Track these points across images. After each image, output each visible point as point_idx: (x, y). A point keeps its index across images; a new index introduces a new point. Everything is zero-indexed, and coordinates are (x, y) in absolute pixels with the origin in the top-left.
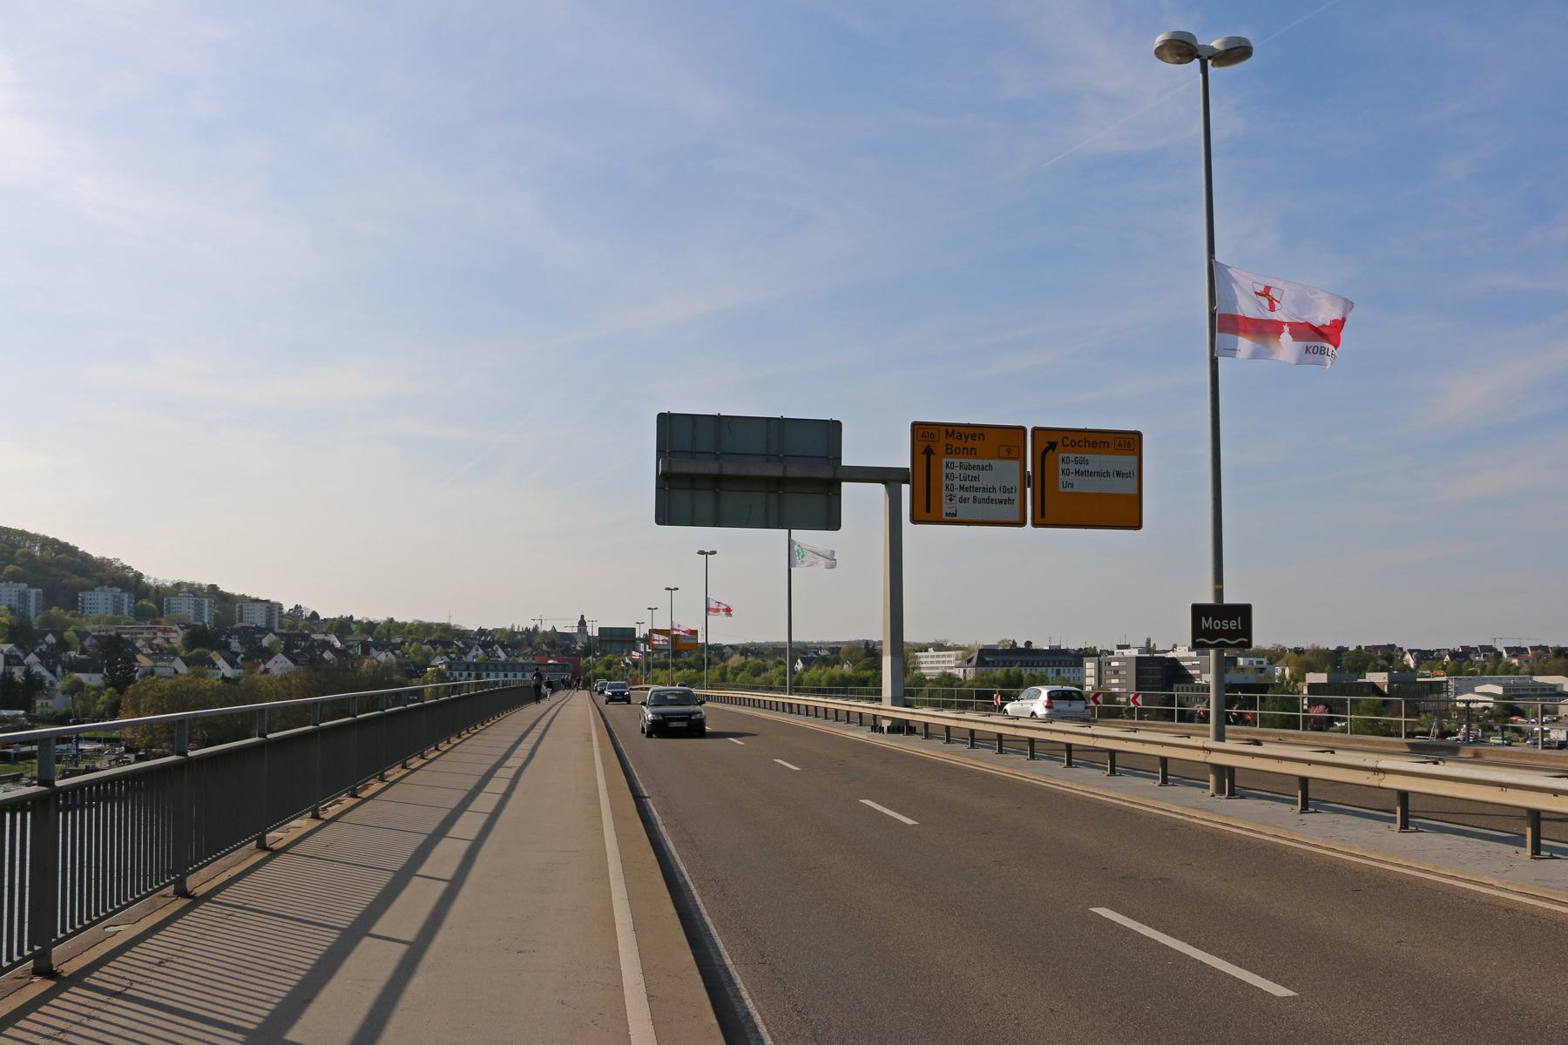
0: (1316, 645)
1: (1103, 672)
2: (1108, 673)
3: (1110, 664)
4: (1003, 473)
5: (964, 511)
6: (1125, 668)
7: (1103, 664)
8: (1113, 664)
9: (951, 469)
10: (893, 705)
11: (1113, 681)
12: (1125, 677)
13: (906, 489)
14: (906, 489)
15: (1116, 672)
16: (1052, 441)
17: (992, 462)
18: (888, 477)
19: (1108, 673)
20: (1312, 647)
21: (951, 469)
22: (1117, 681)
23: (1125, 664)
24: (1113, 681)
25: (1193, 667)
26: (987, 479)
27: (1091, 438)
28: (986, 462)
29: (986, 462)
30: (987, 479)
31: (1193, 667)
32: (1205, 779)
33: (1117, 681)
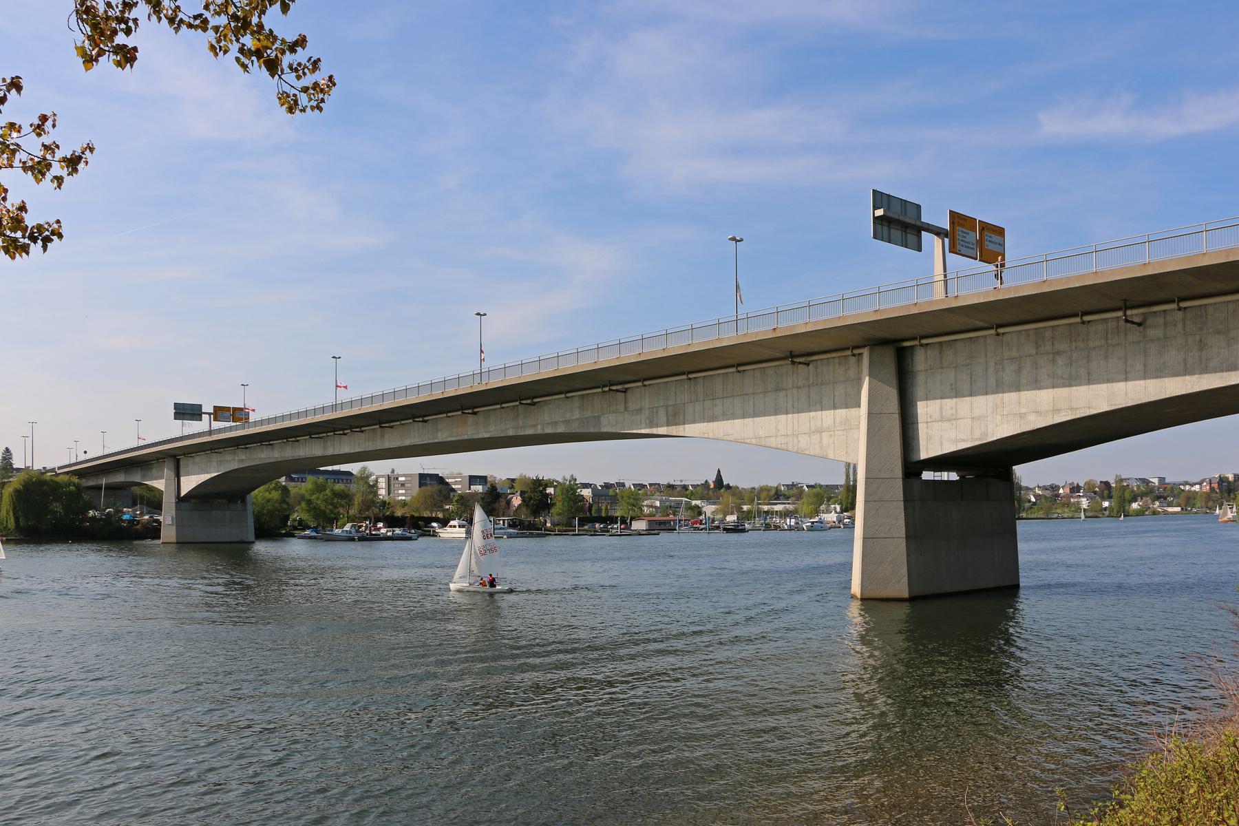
0: (524, 474)
1: (392, 485)
2: (397, 486)
3: (397, 479)
4: (227, 414)
5: (964, 251)
6: (410, 482)
7: (392, 479)
8: (400, 479)
9: (219, 413)
10: (859, 406)
11: (400, 492)
12: (410, 489)
13: (212, 416)
14: (212, 416)
15: (403, 485)
16: (235, 409)
17: (969, 231)
18: (210, 414)
19: (397, 486)
20: (521, 476)
21: (219, 413)
22: (404, 491)
23: (410, 478)
24: (400, 492)
25: (456, 483)
26: (225, 415)
27: (993, 228)
28: (967, 231)
29: (967, 231)
30: (225, 415)
31: (456, 483)
32: (870, 603)
33: (404, 491)
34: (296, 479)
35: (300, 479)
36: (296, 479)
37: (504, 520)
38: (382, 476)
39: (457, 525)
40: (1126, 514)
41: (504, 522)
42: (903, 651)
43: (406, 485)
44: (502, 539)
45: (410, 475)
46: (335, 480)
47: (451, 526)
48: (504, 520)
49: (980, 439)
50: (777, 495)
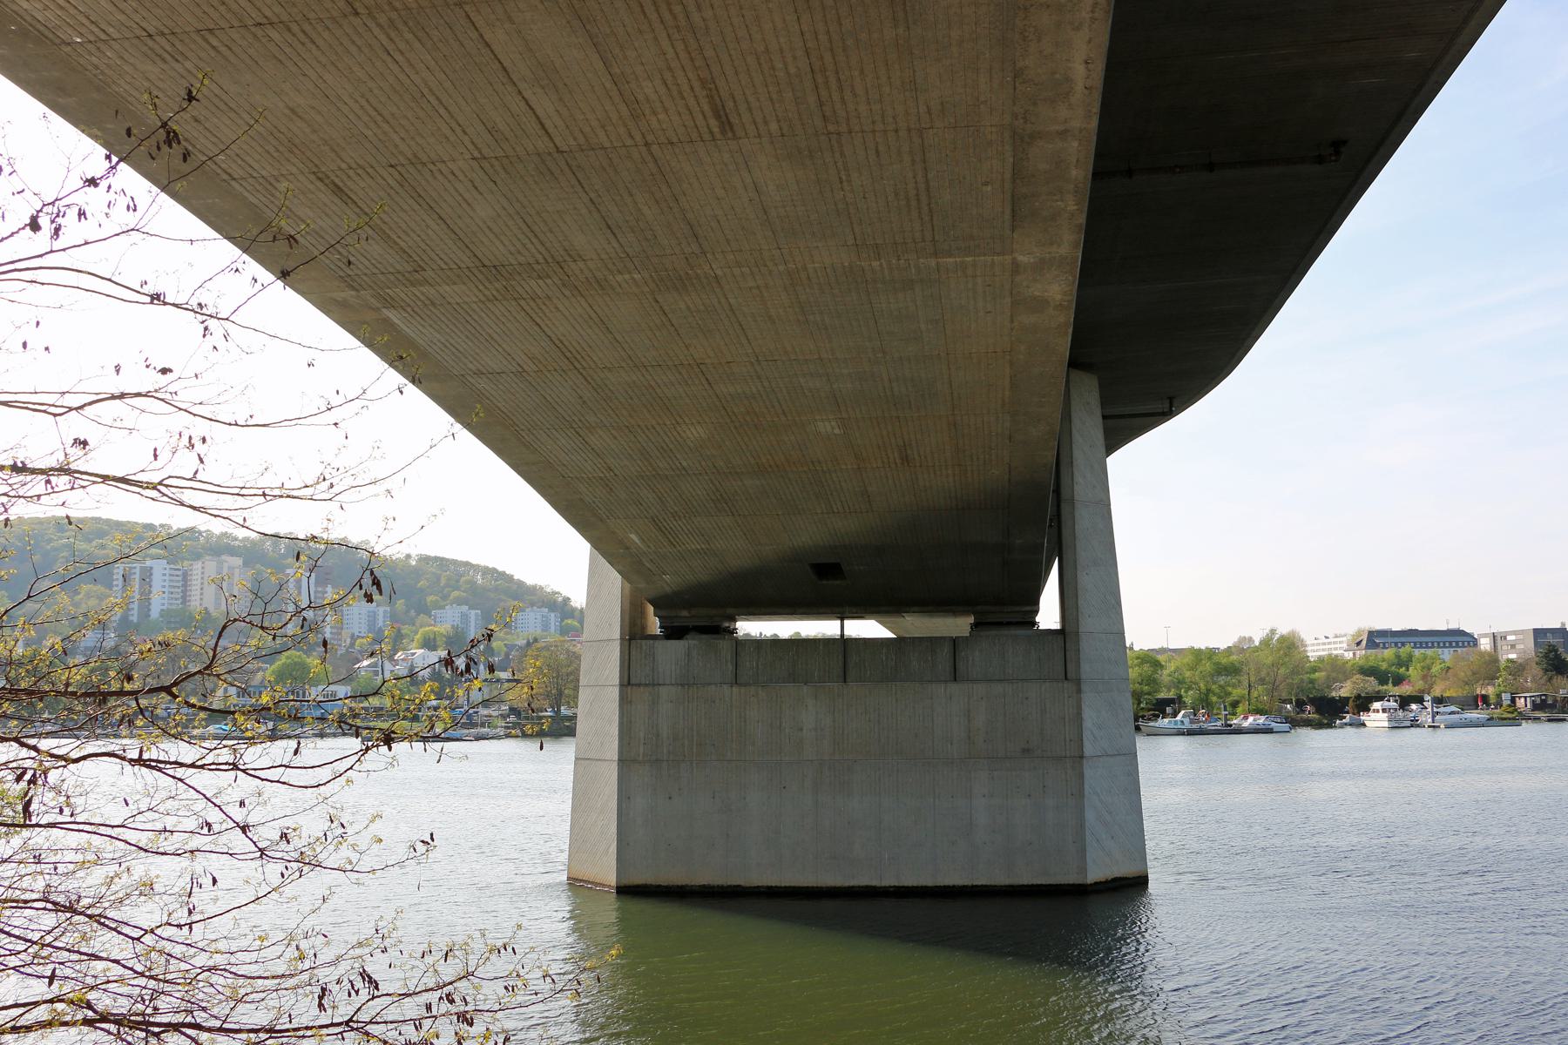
1: (1499, 648)
2: (1505, 648)
3: (1505, 638)
6: (1522, 641)
8: (1509, 638)
15: (1513, 646)
19: (1505, 648)
34: (1381, 645)
35: (1436, 644)
36: (1381, 645)
37: (1526, 698)
38: (1485, 636)
39: (1380, 708)
40: (1228, 717)
41: (1526, 701)
42: (1117, 999)
43: (1517, 647)
44: (1288, 734)
45: (1522, 632)
46: (1415, 643)
47: (1374, 711)
48: (1526, 698)
49: (1075, 276)
50: (654, 658)
